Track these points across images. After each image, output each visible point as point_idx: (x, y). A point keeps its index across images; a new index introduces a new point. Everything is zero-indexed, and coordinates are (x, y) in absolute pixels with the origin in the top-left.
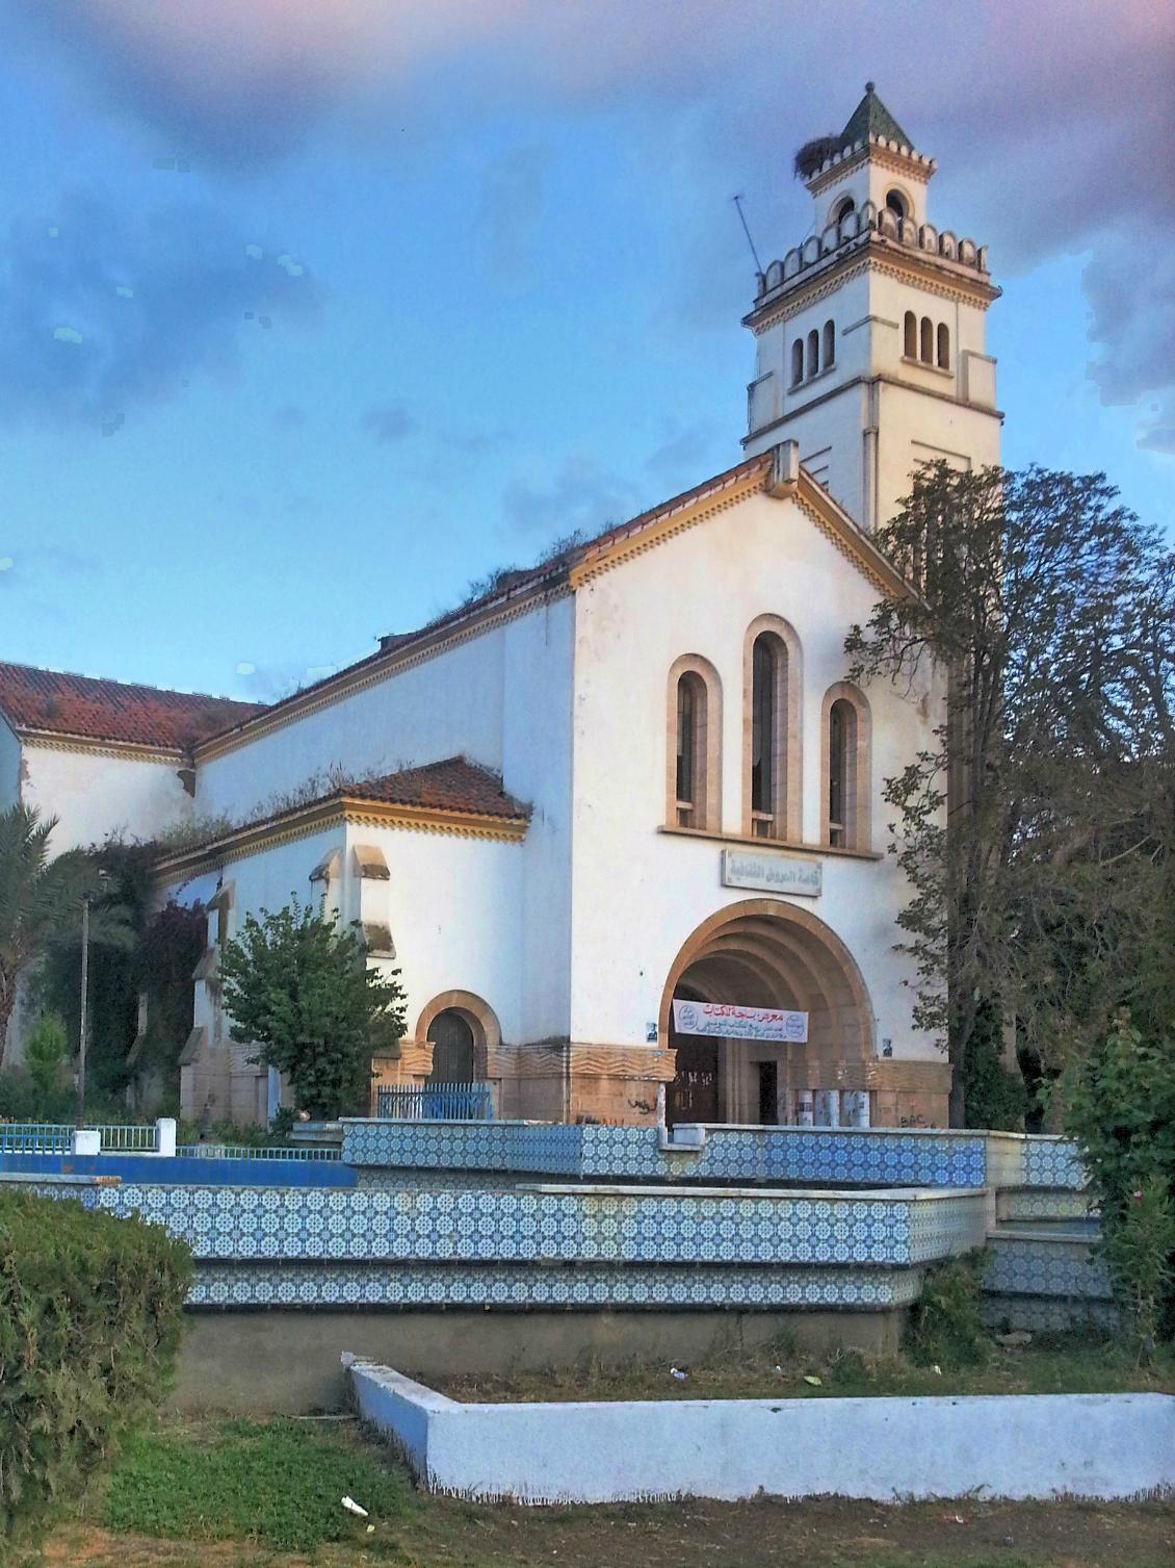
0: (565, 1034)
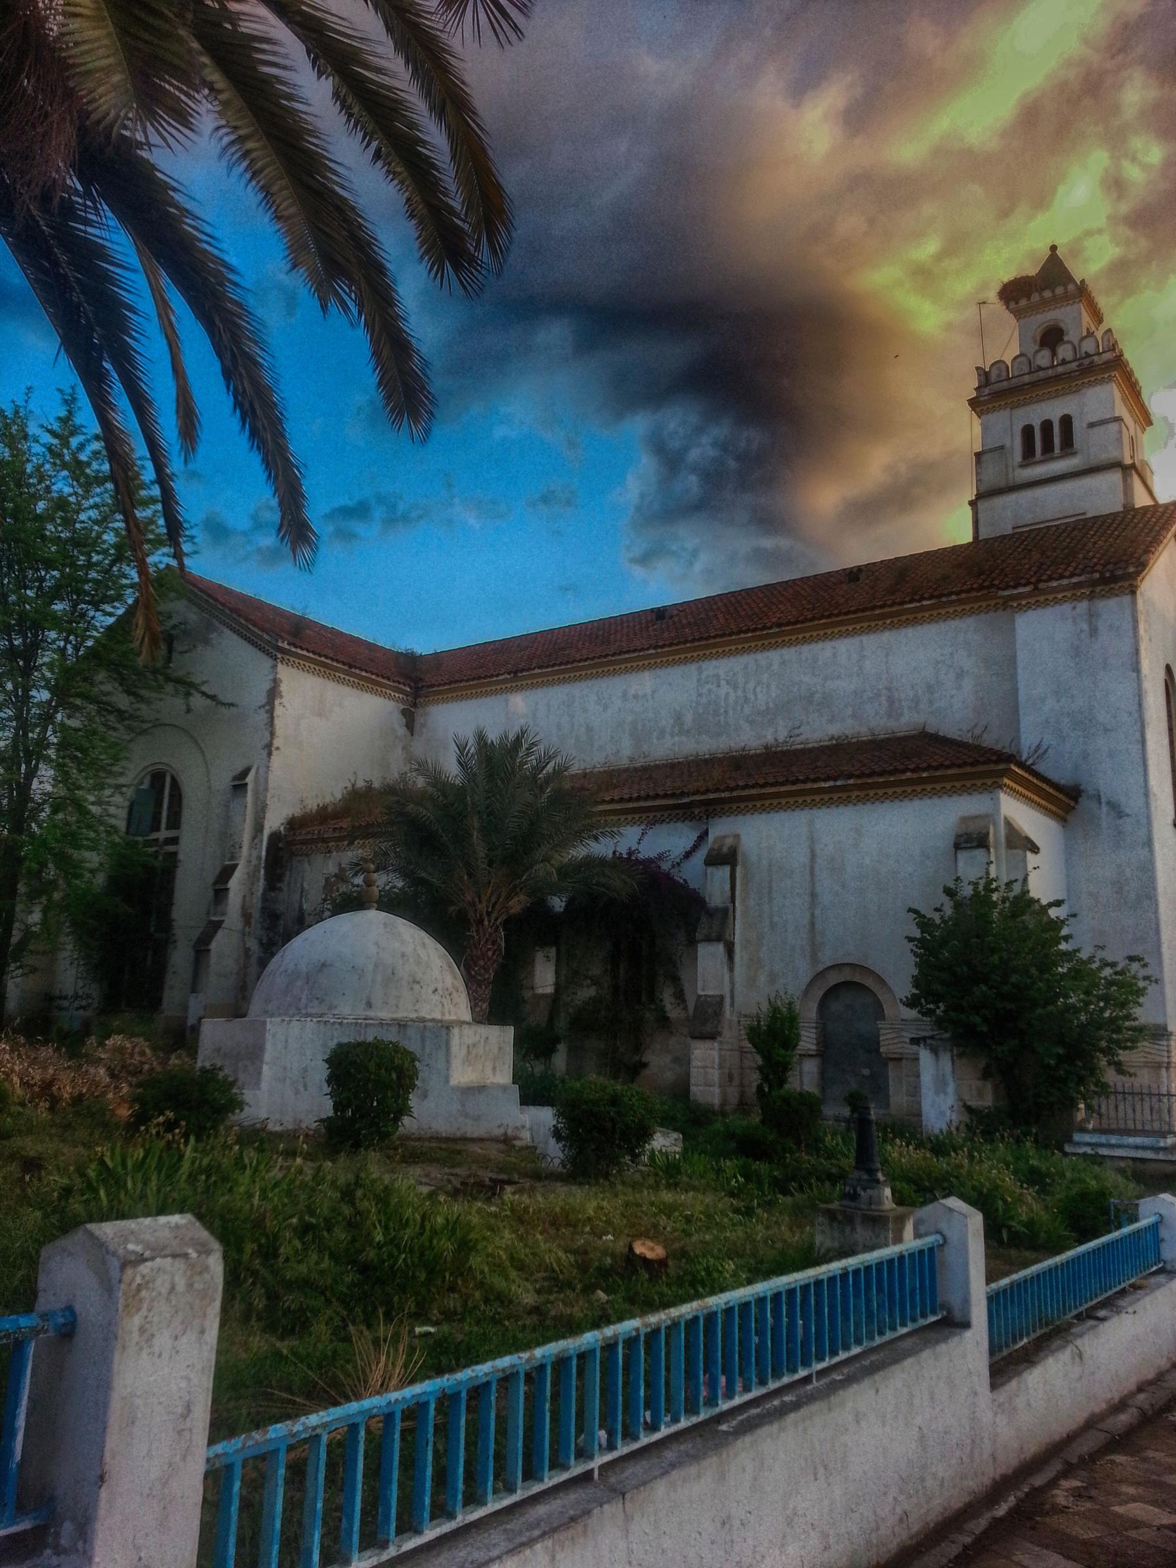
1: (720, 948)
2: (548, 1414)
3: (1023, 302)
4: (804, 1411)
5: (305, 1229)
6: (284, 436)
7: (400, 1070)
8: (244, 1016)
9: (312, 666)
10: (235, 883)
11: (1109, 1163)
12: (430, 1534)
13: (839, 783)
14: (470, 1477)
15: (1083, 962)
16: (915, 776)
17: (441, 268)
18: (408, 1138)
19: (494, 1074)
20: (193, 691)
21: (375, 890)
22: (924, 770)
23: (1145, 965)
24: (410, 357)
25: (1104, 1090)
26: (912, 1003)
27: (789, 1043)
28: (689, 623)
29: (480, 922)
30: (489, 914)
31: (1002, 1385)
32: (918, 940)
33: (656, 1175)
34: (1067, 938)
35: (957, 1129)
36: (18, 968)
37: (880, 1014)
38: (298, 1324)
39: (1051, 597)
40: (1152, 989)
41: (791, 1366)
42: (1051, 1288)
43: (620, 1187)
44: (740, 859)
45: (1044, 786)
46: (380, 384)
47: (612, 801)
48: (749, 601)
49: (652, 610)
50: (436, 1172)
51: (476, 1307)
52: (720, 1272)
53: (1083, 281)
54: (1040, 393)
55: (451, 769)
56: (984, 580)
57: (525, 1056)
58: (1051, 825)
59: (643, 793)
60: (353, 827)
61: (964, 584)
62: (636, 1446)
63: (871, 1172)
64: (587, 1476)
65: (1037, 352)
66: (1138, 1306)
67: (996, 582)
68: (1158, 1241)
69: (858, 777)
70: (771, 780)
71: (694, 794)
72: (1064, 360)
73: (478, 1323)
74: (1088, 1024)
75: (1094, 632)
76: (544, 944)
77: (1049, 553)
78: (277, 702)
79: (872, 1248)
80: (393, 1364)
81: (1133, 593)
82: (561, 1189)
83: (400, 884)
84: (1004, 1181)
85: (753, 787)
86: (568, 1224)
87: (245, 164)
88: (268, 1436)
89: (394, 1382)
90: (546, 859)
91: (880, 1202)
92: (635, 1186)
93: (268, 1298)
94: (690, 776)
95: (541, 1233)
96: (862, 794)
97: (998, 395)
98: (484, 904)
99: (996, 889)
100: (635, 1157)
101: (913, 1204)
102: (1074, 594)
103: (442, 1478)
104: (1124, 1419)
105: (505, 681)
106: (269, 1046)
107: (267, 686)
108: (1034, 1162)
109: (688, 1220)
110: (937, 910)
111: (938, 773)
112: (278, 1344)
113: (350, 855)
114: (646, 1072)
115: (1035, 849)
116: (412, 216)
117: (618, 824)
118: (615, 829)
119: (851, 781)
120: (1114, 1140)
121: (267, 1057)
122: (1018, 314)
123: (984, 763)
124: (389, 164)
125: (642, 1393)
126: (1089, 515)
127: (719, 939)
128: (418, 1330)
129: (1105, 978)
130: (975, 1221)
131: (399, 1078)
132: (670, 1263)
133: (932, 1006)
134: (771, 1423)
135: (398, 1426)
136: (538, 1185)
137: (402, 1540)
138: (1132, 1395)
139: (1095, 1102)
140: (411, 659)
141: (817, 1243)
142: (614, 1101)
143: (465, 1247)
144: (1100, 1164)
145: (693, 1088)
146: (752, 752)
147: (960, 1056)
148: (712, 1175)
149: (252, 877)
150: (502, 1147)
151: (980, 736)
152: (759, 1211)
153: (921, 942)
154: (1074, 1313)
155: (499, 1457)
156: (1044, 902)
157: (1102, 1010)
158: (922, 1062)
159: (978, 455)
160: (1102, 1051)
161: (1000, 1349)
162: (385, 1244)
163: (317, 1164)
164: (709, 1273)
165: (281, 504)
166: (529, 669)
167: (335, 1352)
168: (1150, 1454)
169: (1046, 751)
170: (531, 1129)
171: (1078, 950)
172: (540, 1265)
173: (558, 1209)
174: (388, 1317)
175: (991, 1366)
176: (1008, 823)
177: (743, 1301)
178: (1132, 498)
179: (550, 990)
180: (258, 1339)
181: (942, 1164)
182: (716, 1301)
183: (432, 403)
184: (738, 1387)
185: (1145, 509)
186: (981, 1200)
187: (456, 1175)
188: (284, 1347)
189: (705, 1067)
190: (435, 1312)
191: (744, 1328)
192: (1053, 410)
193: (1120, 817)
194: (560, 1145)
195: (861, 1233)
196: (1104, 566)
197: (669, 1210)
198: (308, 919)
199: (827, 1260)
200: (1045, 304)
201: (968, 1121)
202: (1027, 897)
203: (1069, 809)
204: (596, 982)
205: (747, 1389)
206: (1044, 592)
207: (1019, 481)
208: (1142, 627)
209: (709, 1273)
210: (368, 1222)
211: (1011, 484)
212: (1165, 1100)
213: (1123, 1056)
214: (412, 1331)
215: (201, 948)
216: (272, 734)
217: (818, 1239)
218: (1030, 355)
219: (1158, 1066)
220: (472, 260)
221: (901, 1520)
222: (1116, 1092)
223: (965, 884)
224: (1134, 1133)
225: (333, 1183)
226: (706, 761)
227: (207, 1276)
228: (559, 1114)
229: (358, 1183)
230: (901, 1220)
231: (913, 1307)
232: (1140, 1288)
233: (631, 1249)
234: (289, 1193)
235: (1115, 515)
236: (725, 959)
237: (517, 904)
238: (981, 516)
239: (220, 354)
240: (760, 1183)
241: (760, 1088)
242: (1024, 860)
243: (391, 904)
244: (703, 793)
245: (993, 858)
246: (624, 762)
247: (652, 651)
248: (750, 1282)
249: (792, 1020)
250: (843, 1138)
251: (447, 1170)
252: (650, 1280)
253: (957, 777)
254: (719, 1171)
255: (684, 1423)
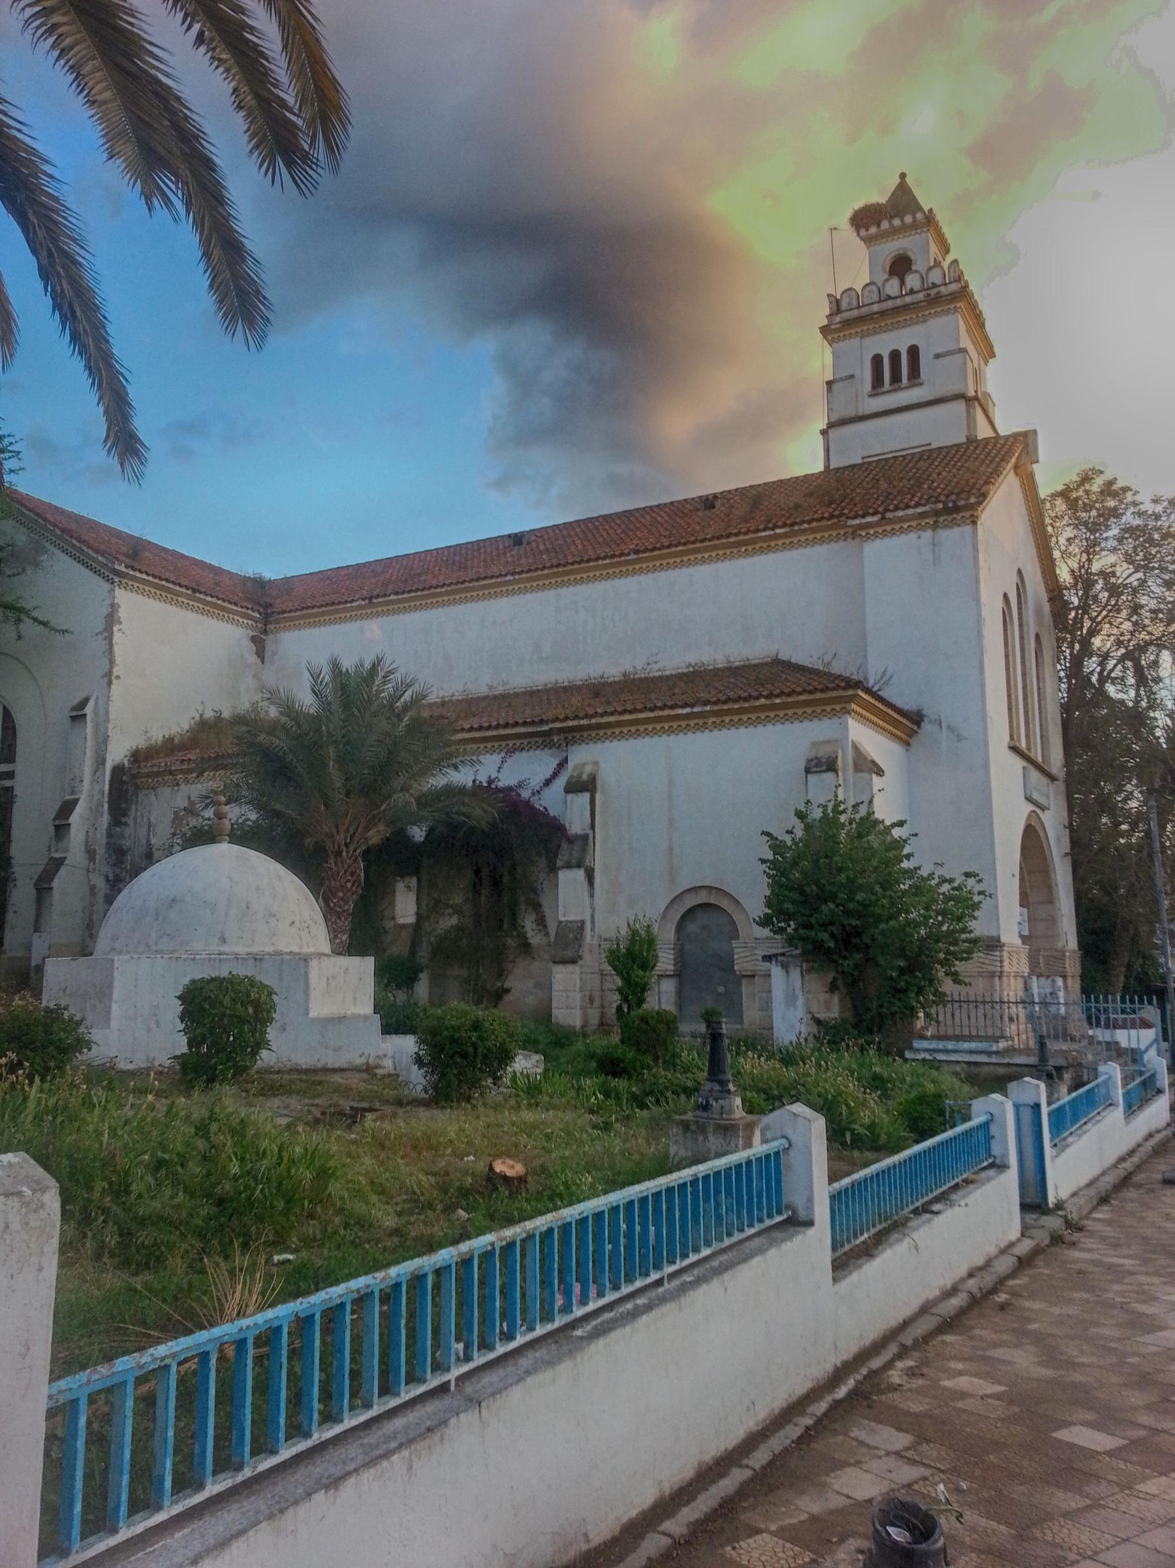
0: (994, 934)
1: (580, 874)
2: (403, 1332)
3: (873, 230)
4: (655, 1313)
5: (159, 1164)
6: (107, 342)
7: (257, 1005)
8: (91, 954)
9: (153, 590)
10: (76, 818)
11: (945, 1067)
12: (286, 1454)
13: (695, 710)
14: (327, 1395)
15: (923, 879)
16: (768, 702)
17: (273, 163)
18: (267, 1070)
19: (355, 1005)
20: (23, 617)
21: (227, 824)
22: (777, 696)
23: (980, 881)
24: (243, 259)
25: (941, 998)
26: (765, 922)
27: (647, 965)
28: (547, 550)
29: (339, 853)
30: (347, 845)
31: (844, 1277)
32: (771, 862)
33: (518, 1096)
34: (908, 857)
35: (806, 1040)
36: (1108, 1222)
37: (734, 933)
38: (152, 1259)
39: (897, 527)
40: (986, 903)
41: (643, 1270)
42: (890, 1186)
43: (481, 1109)
44: (599, 786)
45: (890, 711)
46: (211, 286)
47: (471, 729)
48: (607, 527)
49: (509, 536)
50: (295, 1102)
51: (335, 1233)
52: (578, 1185)
53: (931, 210)
54: (889, 322)
55: (306, 700)
56: (835, 510)
57: (386, 986)
58: (895, 748)
59: (502, 722)
60: (202, 759)
61: (816, 512)
62: (492, 1356)
63: (723, 1083)
64: (444, 1388)
65: (886, 280)
66: (970, 1200)
67: (846, 511)
68: (989, 1138)
69: (715, 703)
70: (629, 707)
71: (553, 721)
72: (912, 289)
73: (338, 1247)
74: (928, 937)
75: (936, 561)
76: (403, 873)
77: (895, 483)
78: (115, 629)
79: (719, 1155)
80: (250, 1292)
81: (974, 523)
82: (423, 1113)
83: (253, 816)
84: (847, 1087)
85: (612, 714)
86: (431, 1148)
87: (51, 40)
88: (114, 1370)
89: (251, 1308)
90: (405, 789)
91: (731, 1112)
92: (496, 1107)
93: (121, 1235)
94: (549, 703)
95: (402, 1158)
96: (718, 720)
97: (848, 323)
98: (342, 835)
99: (844, 811)
100: (497, 1079)
101: (762, 1112)
102: (919, 523)
103: (297, 1399)
104: (956, 1302)
105: (360, 607)
106: (117, 985)
107: (105, 611)
108: (876, 1069)
109: (548, 1137)
110: (788, 832)
111: (789, 700)
112: (132, 1280)
113: (198, 789)
114: (507, 998)
115: (880, 772)
116: (240, 107)
117: (477, 752)
118: (474, 758)
119: (708, 708)
120: (950, 1045)
121: (116, 995)
122: (868, 240)
123: (833, 689)
124: (214, 49)
125: (498, 1304)
126: (934, 446)
127: (579, 865)
128: (276, 1258)
129: (944, 894)
130: (819, 1124)
131: (255, 1012)
132: (529, 1179)
133: (783, 924)
134: (624, 1325)
135: (251, 1352)
136: (400, 1111)
137: (256, 1462)
138: (963, 1280)
139: (933, 1011)
140: (260, 583)
141: (672, 1153)
142: (476, 1026)
143: (323, 1175)
144: (938, 1069)
145: (555, 1012)
146: (611, 680)
147: (809, 971)
148: (573, 1094)
149: (95, 812)
150: (364, 1075)
151: (829, 664)
152: (617, 1125)
153: (773, 864)
154: (911, 1207)
155: (355, 1375)
156: (888, 823)
157: (941, 924)
158: (773, 980)
159: (830, 384)
160: (940, 963)
161: (842, 1246)
162: (242, 1176)
163: (169, 1102)
164: (567, 1187)
165: (106, 412)
166: (385, 595)
167: (190, 1284)
168: (977, 1332)
169: (891, 677)
170: (393, 1058)
171: (919, 868)
172: (401, 1189)
173: (419, 1134)
174: (245, 1246)
175: (833, 1261)
176: (856, 747)
177: (597, 1210)
178: (975, 428)
179: (411, 920)
180: (110, 1275)
181: (790, 1074)
182: (570, 1213)
183: (267, 308)
184: (592, 1292)
185: (987, 441)
186: (827, 1107)
187: (317, 1106)
188: (138, 1282)
189: (566, 991)
190: (294, 1239)
191: (598, 1238)
192: (898, 340)
193: (959, 740)
194: (422, 1071)
195: (714, 1141)
196: (947, 496)
197: (530, 1129)
198: (156, 855)
199: (678, 1167)
200: (894, 232)
201: (816, 1031)
202: (872, 818)
203: (912, 733)
204: (457, 910)
205: (601, 1295)
206: (891, 521)
207: (868, 411)
208: (981, 556)
209: (567, 1187)
210: (224, 1156)
211: (860, 414)
212: (997, 1007)
213: (959, 966)
214: (268, 1260)
215: (43, 887)
216: (112, 662)
217: (673, 1149)
218: (880, 284)
219: (992, 975)
220: (306, 157)
221: (748, 1409)
222: (953, 1001)
223: (815, 807)
224: (970, 1038)
225: (187, 1119)
226: (565, 689)
227: (43, 1214)
228: (421, 1041)
229: (212, 1117)
230: (750, 1127)
231: (760, 1209)
232: (972, 1182)
233: (491, 1168)
234: (140, 1130)
235: (958, 446)
236: (586, 885)
237: (376, 835)
238: (832, 446)
239: (35, 252)
240: (618, 1098)
241: (619, 1008)
242: (870, 784)
243: (244, 837)
244: (561, 721)
245: (841, 782)
246: (484, 690)
247: (509, 578)
248: (606, 1192)
249: (651, 942)
250: (698, 1054)
251: (307, 1101)
252: (510, 1196)
253: (807, 704)
254: (579, 1089)
255: (540, 1331)
